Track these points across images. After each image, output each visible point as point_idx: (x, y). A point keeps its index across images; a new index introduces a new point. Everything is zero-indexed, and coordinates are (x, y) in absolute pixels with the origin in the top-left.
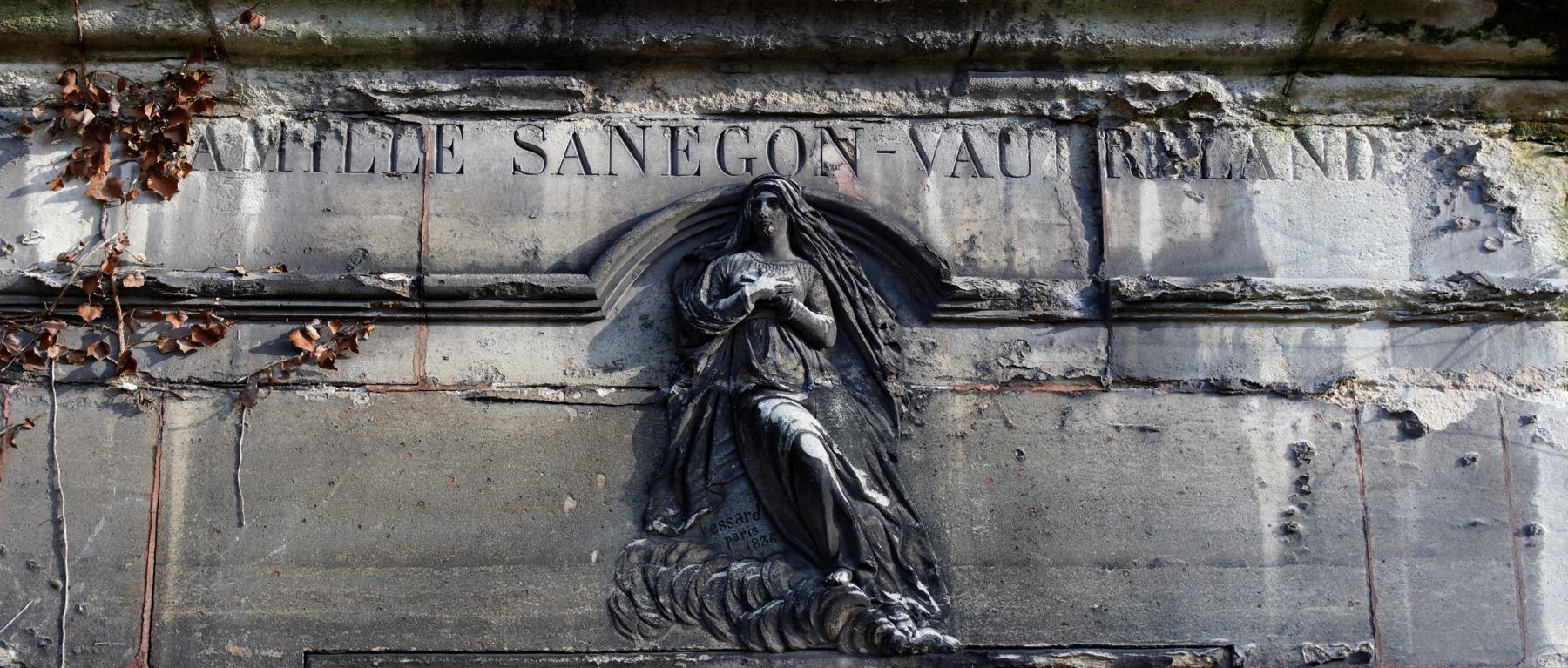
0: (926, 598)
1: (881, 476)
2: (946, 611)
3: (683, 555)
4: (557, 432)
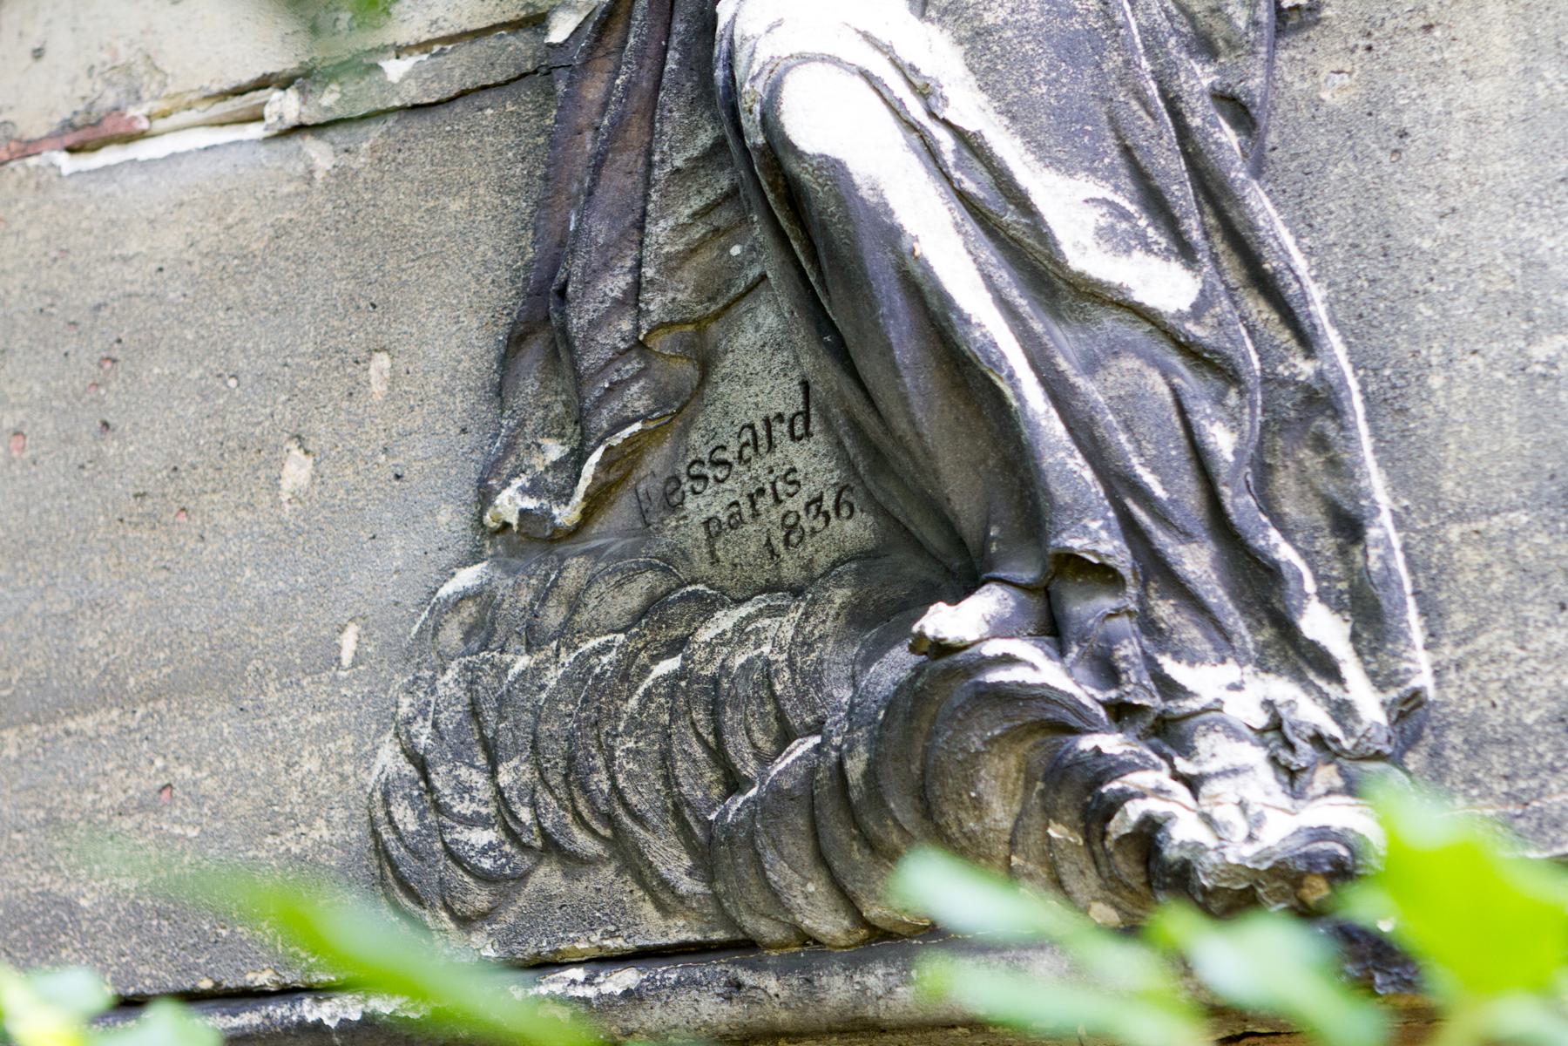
0: (1328, 668)
1: (1181, 193)
2: (1409, 712)
3: (575, 605)
4: (280, 232)
